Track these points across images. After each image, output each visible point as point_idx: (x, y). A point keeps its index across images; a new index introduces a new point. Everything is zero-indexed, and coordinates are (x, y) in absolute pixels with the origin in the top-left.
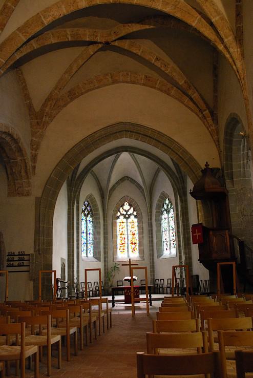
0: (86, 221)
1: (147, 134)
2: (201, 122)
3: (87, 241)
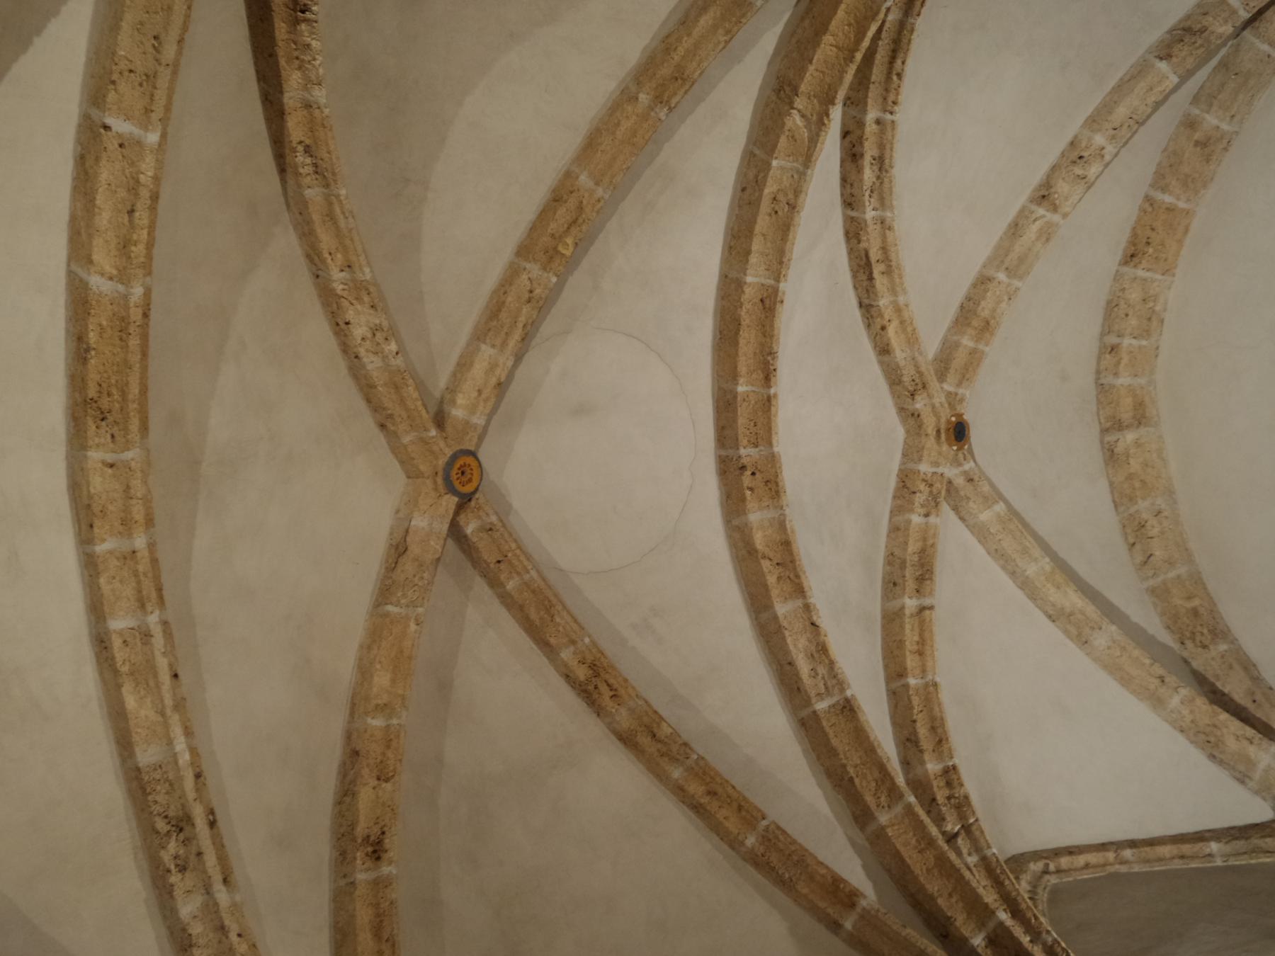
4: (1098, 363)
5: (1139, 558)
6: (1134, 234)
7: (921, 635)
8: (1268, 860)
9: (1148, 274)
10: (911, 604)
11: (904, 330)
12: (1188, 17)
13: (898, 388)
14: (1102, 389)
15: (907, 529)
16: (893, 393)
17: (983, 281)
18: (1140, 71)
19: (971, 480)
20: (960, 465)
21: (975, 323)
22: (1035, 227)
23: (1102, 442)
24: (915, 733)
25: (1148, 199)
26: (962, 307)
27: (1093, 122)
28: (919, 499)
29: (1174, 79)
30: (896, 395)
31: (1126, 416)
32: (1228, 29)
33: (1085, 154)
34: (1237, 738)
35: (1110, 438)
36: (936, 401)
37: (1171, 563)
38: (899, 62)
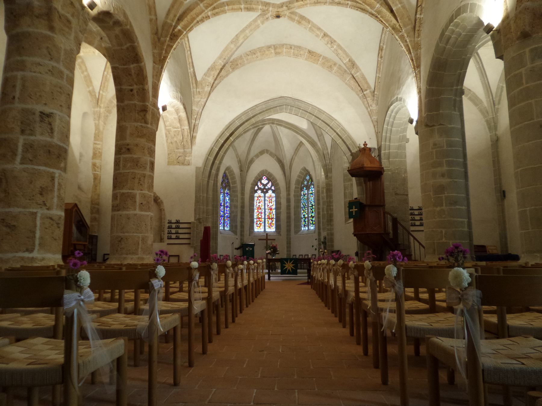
0: (224, 193)
1: (307, 111)
2: (361, 102)
3: (224, 214)
4: (288, 44)
5: (248, 53)
6: (314, 53)
7: (236, 9)
8: (191, 80)
9: (306, 55)
10: (242, 6)
11: (301, 5)
12: (356, 65)
13: (288, 3)
14: (283, 45)
15: (258, 5)
16: (287, 2)
17: (309, 21)
18: (347, 55)
19: (267, 19)
20: (271, 16)
21: (301, 20)
22: (319, 33)
23: (272, 45)
24: (216, 9)
25: (321, 55)
26: (304, 17)
27: (339, 46)
28: (264, 7)
29: (345, 62)
30: (286, 2)
31: (277, 51)
32: (353, 73)
33: (333, 44)
34: (214, 74)
35: (273, 47)
36: (285, 12)
37: (247, 60)
38: (360, 10)
